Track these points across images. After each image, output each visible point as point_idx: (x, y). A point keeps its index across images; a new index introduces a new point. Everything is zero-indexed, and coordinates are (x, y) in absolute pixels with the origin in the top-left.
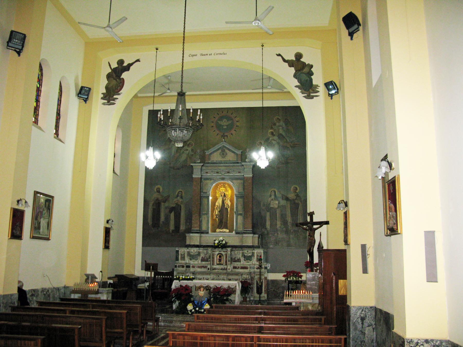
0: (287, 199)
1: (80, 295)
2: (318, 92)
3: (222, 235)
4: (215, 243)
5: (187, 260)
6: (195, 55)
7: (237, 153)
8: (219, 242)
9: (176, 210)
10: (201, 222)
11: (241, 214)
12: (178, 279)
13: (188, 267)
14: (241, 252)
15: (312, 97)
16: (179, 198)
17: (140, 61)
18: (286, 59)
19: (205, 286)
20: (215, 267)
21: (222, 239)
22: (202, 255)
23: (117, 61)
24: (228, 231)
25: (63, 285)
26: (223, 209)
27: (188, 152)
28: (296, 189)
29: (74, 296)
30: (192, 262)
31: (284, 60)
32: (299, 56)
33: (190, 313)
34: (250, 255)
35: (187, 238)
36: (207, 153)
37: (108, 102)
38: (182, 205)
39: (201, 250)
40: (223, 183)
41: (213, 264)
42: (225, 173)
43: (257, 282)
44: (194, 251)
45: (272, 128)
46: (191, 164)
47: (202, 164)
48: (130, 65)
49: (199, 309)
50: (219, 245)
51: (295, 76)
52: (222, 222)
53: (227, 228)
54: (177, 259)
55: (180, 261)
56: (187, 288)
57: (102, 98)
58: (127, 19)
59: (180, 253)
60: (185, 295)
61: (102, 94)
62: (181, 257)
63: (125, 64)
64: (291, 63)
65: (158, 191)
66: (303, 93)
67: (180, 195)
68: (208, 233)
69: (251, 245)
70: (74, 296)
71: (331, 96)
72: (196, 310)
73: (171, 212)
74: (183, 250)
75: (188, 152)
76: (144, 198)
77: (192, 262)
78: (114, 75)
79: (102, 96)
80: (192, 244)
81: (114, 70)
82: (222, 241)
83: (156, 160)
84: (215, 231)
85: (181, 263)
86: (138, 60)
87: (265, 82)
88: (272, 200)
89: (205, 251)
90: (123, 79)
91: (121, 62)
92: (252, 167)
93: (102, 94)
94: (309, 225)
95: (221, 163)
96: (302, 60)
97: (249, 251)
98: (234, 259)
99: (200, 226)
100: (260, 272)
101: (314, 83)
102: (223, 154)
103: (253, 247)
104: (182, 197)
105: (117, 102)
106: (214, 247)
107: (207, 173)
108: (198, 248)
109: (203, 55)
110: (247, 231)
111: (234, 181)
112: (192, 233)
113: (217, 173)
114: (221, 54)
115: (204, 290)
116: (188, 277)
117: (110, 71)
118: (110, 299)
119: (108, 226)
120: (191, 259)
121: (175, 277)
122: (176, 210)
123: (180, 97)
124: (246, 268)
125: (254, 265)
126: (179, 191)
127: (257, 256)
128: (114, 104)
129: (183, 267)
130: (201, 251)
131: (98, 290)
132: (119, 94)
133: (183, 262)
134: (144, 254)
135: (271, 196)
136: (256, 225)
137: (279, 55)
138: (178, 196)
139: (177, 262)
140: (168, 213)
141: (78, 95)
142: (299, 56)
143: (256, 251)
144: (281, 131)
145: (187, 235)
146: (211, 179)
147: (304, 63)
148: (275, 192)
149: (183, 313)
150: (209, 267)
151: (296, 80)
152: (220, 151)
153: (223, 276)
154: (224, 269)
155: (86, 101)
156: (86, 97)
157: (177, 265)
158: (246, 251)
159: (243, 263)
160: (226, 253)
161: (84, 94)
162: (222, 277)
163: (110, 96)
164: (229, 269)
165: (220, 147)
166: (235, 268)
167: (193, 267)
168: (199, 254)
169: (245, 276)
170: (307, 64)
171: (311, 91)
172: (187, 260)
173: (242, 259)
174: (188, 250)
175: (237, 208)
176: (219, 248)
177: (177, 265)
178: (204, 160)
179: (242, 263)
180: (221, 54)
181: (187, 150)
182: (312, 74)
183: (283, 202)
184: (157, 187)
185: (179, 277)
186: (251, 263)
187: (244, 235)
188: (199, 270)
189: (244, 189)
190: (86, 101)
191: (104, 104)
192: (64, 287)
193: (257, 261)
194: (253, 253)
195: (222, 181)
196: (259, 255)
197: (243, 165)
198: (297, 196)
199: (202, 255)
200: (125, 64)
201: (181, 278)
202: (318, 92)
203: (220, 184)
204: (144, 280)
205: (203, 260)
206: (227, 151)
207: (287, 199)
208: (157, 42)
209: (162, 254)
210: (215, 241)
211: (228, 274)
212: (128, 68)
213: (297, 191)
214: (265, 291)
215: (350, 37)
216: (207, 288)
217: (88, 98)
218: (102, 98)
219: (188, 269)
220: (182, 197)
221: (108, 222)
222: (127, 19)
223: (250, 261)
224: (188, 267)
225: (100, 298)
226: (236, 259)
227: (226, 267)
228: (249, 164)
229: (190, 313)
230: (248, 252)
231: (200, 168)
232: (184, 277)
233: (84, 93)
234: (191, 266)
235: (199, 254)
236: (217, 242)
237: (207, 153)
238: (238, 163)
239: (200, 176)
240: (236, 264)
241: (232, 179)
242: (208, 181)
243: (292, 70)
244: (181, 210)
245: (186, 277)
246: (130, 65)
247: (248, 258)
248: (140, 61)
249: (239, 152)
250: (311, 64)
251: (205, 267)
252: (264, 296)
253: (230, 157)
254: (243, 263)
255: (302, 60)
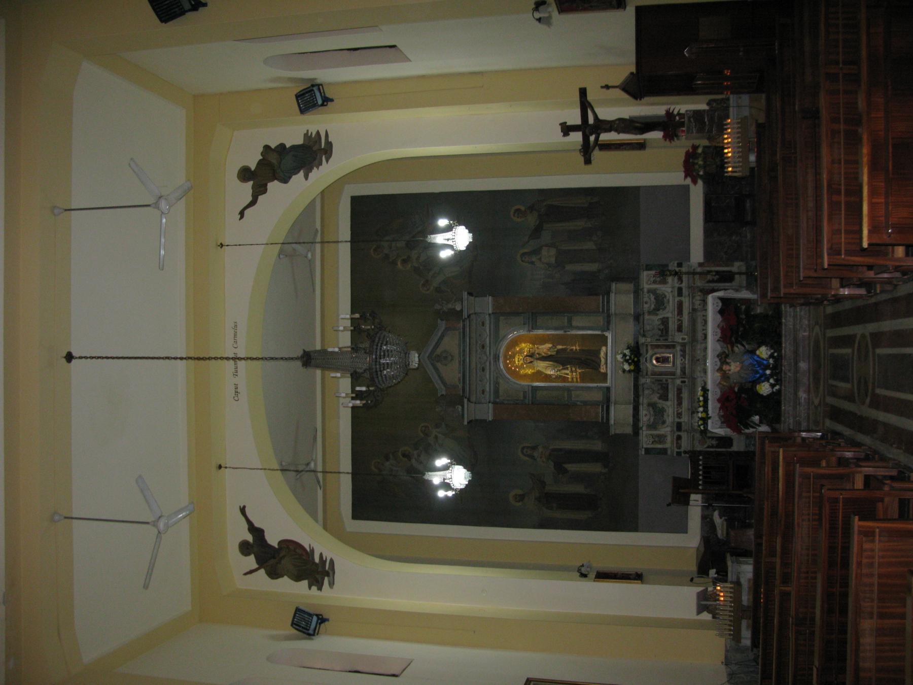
0: (537, 232)
1: (744, 623)
2: (318, 133)
3: (612, 356)
4: (630, 371)
5: (666, 430)
6: (236, 388)
7: (443, 328)
8: (627, 361)
9: (560, 459)
10: (585, 403)
11: (570, 321)
12: (705, 420)
13: (679, 427)
14: (647, 317)
15: (329, 145)
16: (535, 454)
17: (244, 507)
18: (250, 199)
19: (719, 363)
20: (679, 371)
21: (621, 356)
22: (655, 398)
23: (241, 540)
24: (604, 349)
25: (723, 667)
26: (559, 359)
27: (440, 435)
28: (518, 210)
29: (746, 638)
30: (670, 417)
31: (253, 203)
32: (245, 174)
33: (777, 387)
34: (652, 297)
35: (618, 432)
36: (442, 391)
37: (328, 575)
38: (551, 447)
39: (644, 400)
40: (506, 358)
41: (673, 374)
42: (485, 353)
43: (709, 282)
44: (645, 415)
45: (394, 263)
46: (466, 423)
47: (466, 401)
48: (252, 528)
49: (767, 367)
50: (633, 361)
51: (285, 180)
52: (588, 361)
53: (599, 351)
54: (664, 451)
55: (668, 445)
56: (725, 400)
57: (320, 589)
58: (140, 476)
59: (649, 446)
60: (739, 403)
61: (310, 588)
62: (660, 442)
63: (250, 538)
64: (260, 190)
65: (521, 498)
66: (321, 164)
67: (529, 452)
68: (608, 389)
69: (632, 296)
70: (746, 638)
71: (326, 100)
72: (771, 376)
73: (566, 471)
74: (645, 439)
75: (440, 435)
76: (534, 527)
77: (670, 417)
78: (272, 561)
79: (314, 588)
80: (631, 420)
81: (262, 562)
82: (625, 355)
83: (451, 464)
84: (605, 375)
85: (672, 441)
86: (243, 510)
87: (299, 242)
88: (540, 259)
89: (646, 392)
90: (280, 543)
91: (245, 548)
92: (472, 298)
93: (310, 588)
94: (588, 133)
95: (464, 361)
96: (253, 169)
97: (645, 300)
98: (662, 330)
99: (595, 404)
100: (688, 273)
101: (300, 141)
102: (445, 358)
103: (637, 292)
104: (534, 448)
105: (328, 555)
106: (637, 370)
107: (483, 392)
108: (641, 408)
109: (237, 372)
110: (603, 306)
111: (502, 333)
112: (608, 419)
113: (483, 370)
114: (235, 335)
115: (728, 364)
116: (701, 398)
117: (262, 572)
118: (751, 560)
119: (592, 575)
120: (664, 422)
121: (702, 427)
122: (560, 459)
123: (313, 362)
124: (680, 305)
125: (673, 288)
126: (520, 454)
127: (655, 282)
128: (332, 562)
129: (679, 438)
130: (645, 401)
131: (732, 582)
132: (312, 551)
133: (669, 438)
134: (652, 528)
135: (532, 263)
136: (594, 288)
137: (242, 214)
138: (532, 457)
139: (669, 452)
140: (564, 478)
141: (309, 635)
142: (245, 174)
143: (646, 287)
144: (401, 244)
145: (612, 432)
146: (497, 383)
147: (260, 163)
148: (524, 254)
149: (779, 403)
150: (678, 382)
151: (295, 178)
152: (439, 365)
153: (699, 352)
154: (683, 351)
155: (322, 620)
156: (315, 618)
157: (676, 450)
158: (646, 306)
159: (669, 312)
160: (649, 347)
161: (309, 623)
162: (699, 353)
163: (315, 571)
164: (683, 339)
165: (431, 367)
166: (680, 329)
167: (679, 415)
168: (652, 405)
169: (698, 302)
170: (261, 158)
171: (315, 148)
172: (666, 430)
173: (662, 314)
174: (644, 428)
175: (556, 329)
176: (639, 361)
177: (676, 450)
178: (456, 398)
179: (669, 315)
180: (235, 335)
181: (436, 437)
182: (282, 146)
183: (546, 237)
184: (511, 499)
185: (702, 419)
186: (669, 296)
187: (613, 310)
188: (685, 404)
189: (517, 314)
190: (322, 620)
191: (331, 584)
192: (726, 665)
193: (664, 282)
194: (649, 291)
195: (501, 360)
196: (652, 279)
197: (469, 316)
198: (532, 208)
199: (655, 398)
200: (250, 538)
201: (704, 415)
202: (318, 133)
203: (506, 365)
204: (707, 520)
205: (665, 397)
206: (439, 351)
207: (537, 232)
208: (207, 465)
209: (653, 481)
210: (624, 371)
211: (694, 340)
212: (257, 532)
213: (523, 208)
214: (727, 266)
215: (201, 9)
216: (723, 358)
217: (317, 615)
218: (320, 589)
219: (684, 427)
220: (534, 448)
221: (584, 576)
222: (140, 476)
223: (665, 296)
224: (679, 427)
225: (749, 580)
226: (662, 327)
227: (678, 348)
228: (465, 303)
229: (777, 387)
230: (646, 303)
231: (473, 405)
232: (701, 409)
233: (307, 623)
234: (677, 420)
235: (652, 405)
236: (626, 367)
237: (442, 391)
238: (464, 328)
239: (490, 405)
240: (673, 326)
241: (497, 338)
242: (501, 393)
243: (274, 186)
244: (561, 450)
245: (701, 404)
246: (252, 528)
247: (660, 301)
248: (244, 507)
249: (442, 325)
250: (261, 149)
251: (679, 390)
252: (737, 266)
253: (451, 343)
254: (669, 312)
255: (253, 169)
